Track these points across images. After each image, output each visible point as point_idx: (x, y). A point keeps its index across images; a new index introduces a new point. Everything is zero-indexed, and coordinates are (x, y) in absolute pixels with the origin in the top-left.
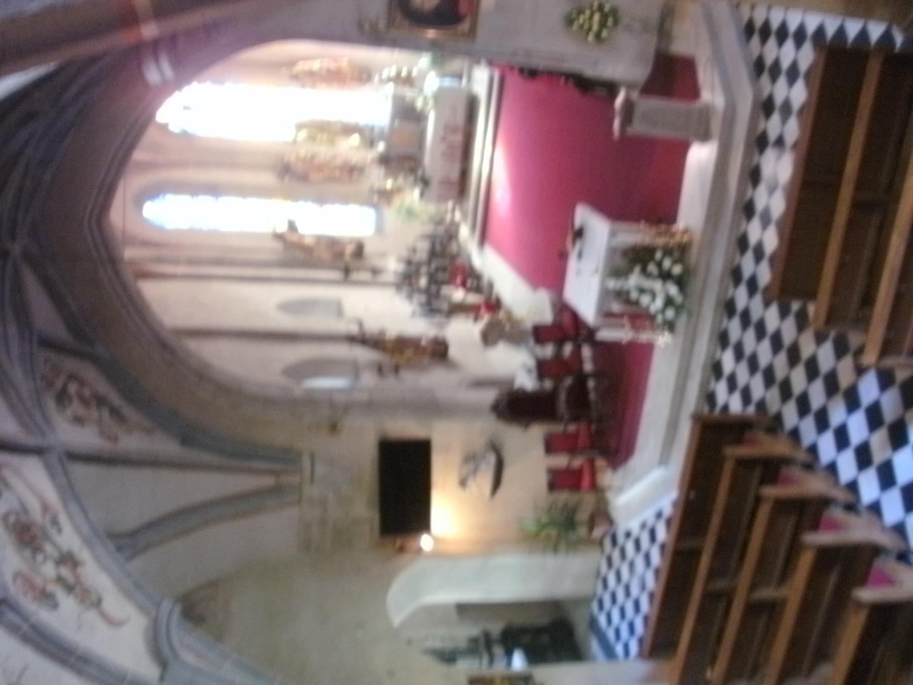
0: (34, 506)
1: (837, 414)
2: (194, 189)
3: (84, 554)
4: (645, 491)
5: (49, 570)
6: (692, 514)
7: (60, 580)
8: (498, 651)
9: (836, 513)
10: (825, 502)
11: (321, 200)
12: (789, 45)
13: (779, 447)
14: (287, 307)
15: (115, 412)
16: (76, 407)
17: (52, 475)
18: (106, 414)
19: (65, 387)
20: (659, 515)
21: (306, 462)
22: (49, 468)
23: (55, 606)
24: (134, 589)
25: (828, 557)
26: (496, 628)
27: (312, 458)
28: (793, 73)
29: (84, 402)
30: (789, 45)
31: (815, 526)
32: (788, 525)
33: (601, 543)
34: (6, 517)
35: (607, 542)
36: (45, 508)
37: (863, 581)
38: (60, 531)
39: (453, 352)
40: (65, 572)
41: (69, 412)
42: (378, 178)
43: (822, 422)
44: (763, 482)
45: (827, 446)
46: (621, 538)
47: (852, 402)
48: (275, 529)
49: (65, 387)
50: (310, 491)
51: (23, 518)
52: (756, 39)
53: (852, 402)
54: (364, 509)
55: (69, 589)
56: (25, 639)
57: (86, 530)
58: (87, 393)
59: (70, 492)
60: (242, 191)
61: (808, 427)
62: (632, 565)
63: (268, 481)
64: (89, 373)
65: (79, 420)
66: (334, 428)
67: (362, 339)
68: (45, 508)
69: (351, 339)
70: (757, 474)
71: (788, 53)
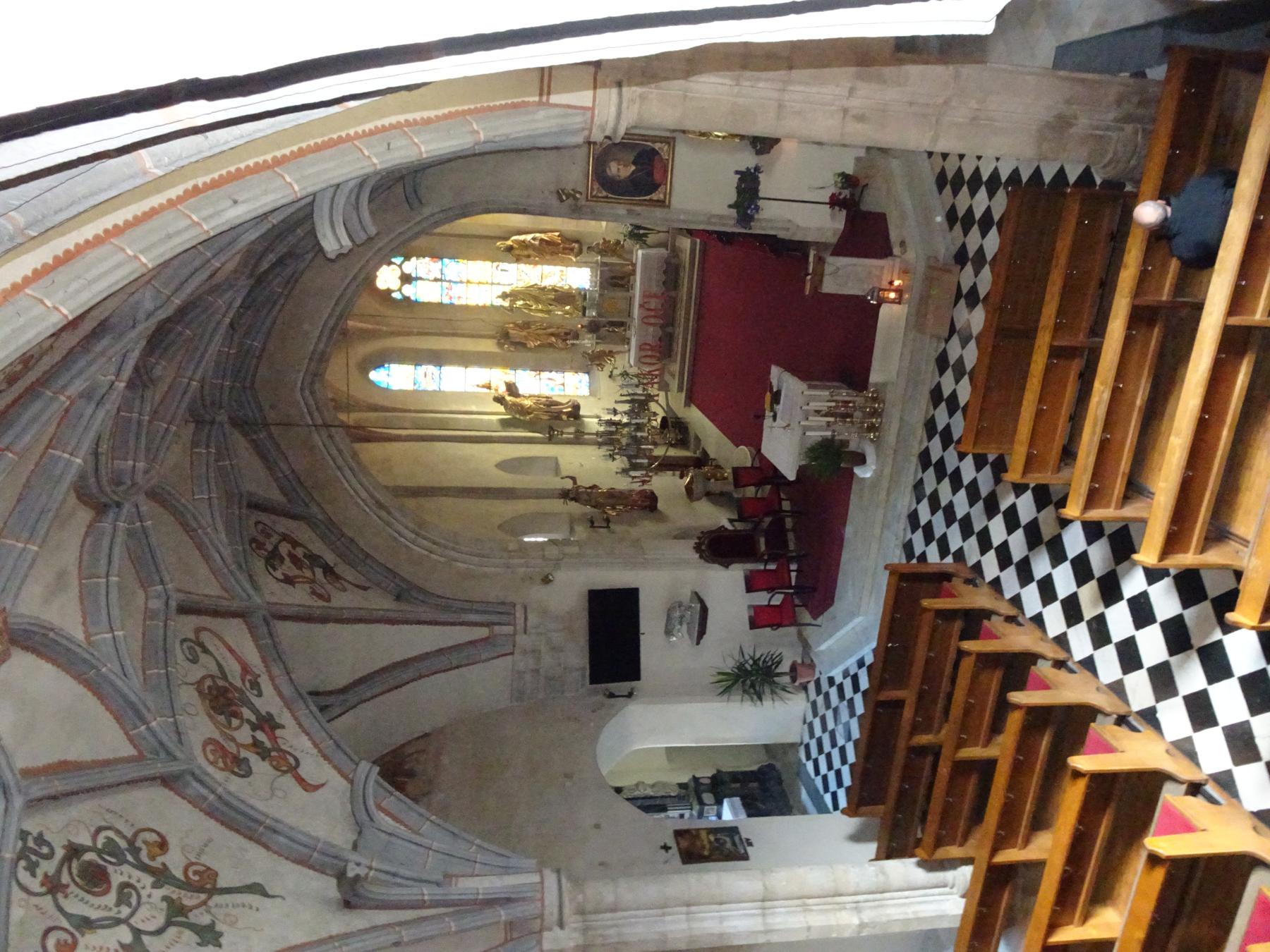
0: (233, 668)
1: (1041, 566)
2: (418, 358)
3: (285, 718)
4: (850, 635)
5: (244, 735)
6: (891, 661)
7: (256, 744)
8: (708, 798)
9: (1043, 669)
10: (1031, 658)
11: (538, 368)
12: (982, 193)
13: (980, 599)
14: (504, 465)
15: (328, 570)
16: (288, 568)
17: (255, 638)
18: (319, 571)
19: (276, 547)
20: (861, 664)
21: (519, 614)
22: (252, 630)
23: (248, 773)
24: (338, 753)
25: (1039, 717)
26: (706, 773)
27: (525, 608)
28: (986, 223)
29: (295, 560)
30: (982, 193)
31: (1021, 686)
32: (994, 680)
33: (804, 688)
34: (200, 683)
35: (812, 687)
36: (246, 669)
37: (1076, 748)
38: (260, 695)
39: (660, 505)
40: (261, 736)
41: (279, 574)
42: (588, 342)
43: (1025, 574)
44: (965, 636)
45: (1031, 598)
46: (825, 685)
47: (1058, 556)
48: (486, 683)
49: (276, 547)
50: (521, 640)
51: (221, 683)
52: (948, 190)
53: (1058, 556)
54: (577, 656)
55: (264, 754)
56: (211, 813)
57: (287, 690)
58: (299, 552)
59: (273, 653)
60: (465, 359)
61: (1010, 580)
62: (836, 711)
63: (483, 632)
64: (303, 533)
65: (289, 580)
66: (546, 580)
67: (571, 495)
68: (246, 669)
69: (565, 495)
70: (958, 625)
71: (981, 201)
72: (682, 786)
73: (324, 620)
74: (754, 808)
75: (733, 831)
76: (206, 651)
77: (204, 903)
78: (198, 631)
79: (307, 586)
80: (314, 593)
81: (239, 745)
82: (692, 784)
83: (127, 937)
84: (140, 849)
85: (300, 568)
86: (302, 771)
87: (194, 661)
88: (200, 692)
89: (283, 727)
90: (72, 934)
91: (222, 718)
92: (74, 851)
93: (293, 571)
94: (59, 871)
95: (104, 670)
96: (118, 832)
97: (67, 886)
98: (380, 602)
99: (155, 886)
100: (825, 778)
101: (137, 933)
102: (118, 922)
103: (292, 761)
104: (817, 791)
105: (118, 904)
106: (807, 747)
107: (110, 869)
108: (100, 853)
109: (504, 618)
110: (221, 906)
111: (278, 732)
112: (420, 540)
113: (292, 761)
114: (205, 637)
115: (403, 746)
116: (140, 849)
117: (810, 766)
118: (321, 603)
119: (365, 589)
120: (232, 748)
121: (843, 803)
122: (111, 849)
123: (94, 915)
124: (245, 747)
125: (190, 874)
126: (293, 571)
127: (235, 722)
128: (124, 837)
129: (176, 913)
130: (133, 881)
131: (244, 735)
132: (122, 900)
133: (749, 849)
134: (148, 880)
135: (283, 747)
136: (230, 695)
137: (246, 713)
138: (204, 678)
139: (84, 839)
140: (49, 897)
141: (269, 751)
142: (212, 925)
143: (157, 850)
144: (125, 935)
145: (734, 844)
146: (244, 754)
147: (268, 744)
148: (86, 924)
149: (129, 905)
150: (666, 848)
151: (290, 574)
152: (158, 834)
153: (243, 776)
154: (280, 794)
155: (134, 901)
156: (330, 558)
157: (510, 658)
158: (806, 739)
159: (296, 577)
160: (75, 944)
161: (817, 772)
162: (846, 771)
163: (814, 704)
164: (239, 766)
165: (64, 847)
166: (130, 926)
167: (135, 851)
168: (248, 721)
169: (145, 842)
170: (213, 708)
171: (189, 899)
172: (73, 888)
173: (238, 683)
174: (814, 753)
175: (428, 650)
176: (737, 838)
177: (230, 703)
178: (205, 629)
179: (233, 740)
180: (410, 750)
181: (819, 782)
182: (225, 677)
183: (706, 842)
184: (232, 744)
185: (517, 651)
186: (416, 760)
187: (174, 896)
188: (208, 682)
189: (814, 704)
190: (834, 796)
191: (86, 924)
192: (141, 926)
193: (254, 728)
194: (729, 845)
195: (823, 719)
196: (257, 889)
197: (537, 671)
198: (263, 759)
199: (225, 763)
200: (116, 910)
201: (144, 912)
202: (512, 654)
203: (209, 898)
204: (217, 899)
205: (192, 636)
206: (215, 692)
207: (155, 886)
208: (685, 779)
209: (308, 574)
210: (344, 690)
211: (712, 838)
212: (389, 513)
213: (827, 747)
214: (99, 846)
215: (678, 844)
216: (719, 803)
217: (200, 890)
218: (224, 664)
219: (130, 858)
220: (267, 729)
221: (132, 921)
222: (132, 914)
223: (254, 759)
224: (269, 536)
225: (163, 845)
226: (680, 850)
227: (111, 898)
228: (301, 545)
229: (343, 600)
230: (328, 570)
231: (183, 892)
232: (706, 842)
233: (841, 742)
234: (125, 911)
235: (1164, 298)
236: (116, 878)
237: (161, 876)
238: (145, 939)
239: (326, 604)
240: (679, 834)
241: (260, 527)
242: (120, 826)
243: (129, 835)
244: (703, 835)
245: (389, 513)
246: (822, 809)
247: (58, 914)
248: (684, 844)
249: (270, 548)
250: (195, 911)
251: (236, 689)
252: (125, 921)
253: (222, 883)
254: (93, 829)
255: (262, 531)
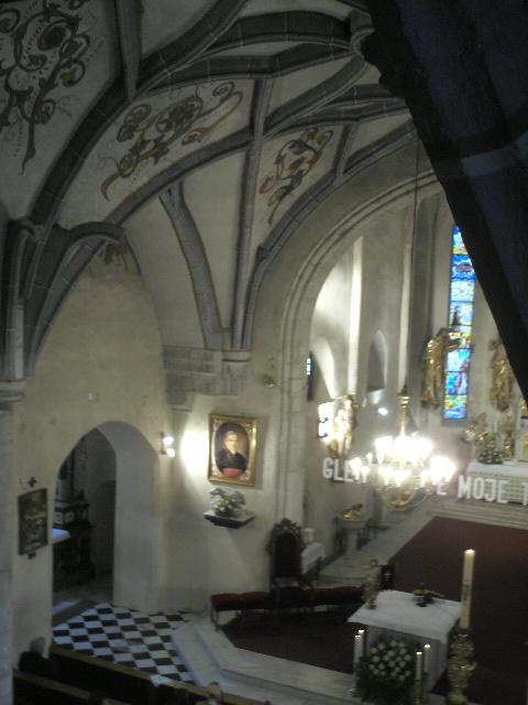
0: (208, 122)
7: (144, 143)
8: (70, 517)
16: (291, 158)
19: (310, 148)
21: (243, 355)
26: (90, 515)
34: (197, 98)
36: (205, 131)
38: (184, 143)
40: (150, 146)
41: (286, 151)
46: (164, 632)
49: (310, 148)
51: (196, 113)
55: (135, 150)
58: (305, 166)
62: (139, 641)
64: (322, 169)
65: (280, 159)
68: (205, 131)
72: (81, 496)
73: (244, 186)
74: (61, 551)
75: (44, 540)
76: (223, 101)
77: (24, 117)
78: (240, 94)
79: (274, 174)
80: (268, 180)
81: (143, 131)
82: (82, 503)
83: (6, 65)
84: (69, 67)
85: (291, 167)
86: (120, 179)
87: (215, 93)
88: (189, 99)
89: (156, 162)
90: (11, 29)
91: (167, 116)
92: (73, 23)
93: (288, 162)
94: (61, 14)
95: (212, 35)
96: (84, 51)
97: (48, 21)
98: (257, 235)
99: (41, 80)
100: (80, 625)
101: (8, 72)
102: (18, 58)
103: (127, 172)
104: (71, 617)
105: (31, 57)
106: (108, 611)
107: (58, 49)
108: (71, 40)
109: (238, 343)
110: (21, 129)
111: (152, 159)
112: (311, 268)
113: (127, 172)
114: (235, 99)
115: (132, 251)
116: (69, 67)
117: (92, 612)
118: (259, 185)
119: (270, 221)
120: (142, 125)
121: (61, 640)
122: (74, 46)
123: (25, 43)
124: (142, 135)
125: (49, 104)
126: (288, 162)
127: (162, 127)
128: (80, 55)
129: (20, 97)
130: (47, 65)
131: (152, 134)
132: (33, 60)
133: (26, 556)
134: (46, 75)
135: (139, 164)
136: (185, 121)
137: (171, 133)
138: (201, 101)
139: (82, 28)
140: (41, 9)
141: (137, 154)
142: (8, 124)
143: (67, 79)
144: (9, 62)
145: (34, 541)
146: (137, 135)
147: (143, 152)
148: (18, 38)
149: (29, 65)
150: (32, 482)
151: (285, 160)
152: (79, 79)
153: (119, 135)
154: (102, 164)
155: (33, 67)
156: (298, 192)
157: (202, 346)
158: (117, 611)
159: (283, 164)
160: (6, 31)
161: (88, 619)
162: (86, 646)
163: (145, 621)
164: (126, 132)
165: (77, 16)
166: (14, 67)
167: (67, 65)
168: (163, 136)
169: (75, 70)
170: (175, 110)
171: (28, 106)
172: (47, 24)
173: (195, 126)
174: (104, 617)
175: (216, 288)
176: (38, 544)
177: (179, 122)
178: (241, 100)
179: (149, 126)
180: (128, 257)
181: (78, 619)
182: (200, 116)
183: (36, 516)
184: (145, 125)
185: (208, 352)
186: (120, 265)
187: (32, 95)
188: (196, 104)
189: (145, 621)
190: (65, 633)
191: (18, 38)
192: (13, 74)
193: (157, 141)
194: (33, 537)
195: (132, 628)
196: (31, 152)
197: (189, 367)
198: (131, 150)
199: (130, 121)
200: (27, 55)
201: (23, 74)
202: (206, 348)
203: (27, 119)
204: (26, 124)
205: (236, 89)
206: (189, 109)
207: (41, 80)
208: (87, 496)
209: (285, 174)
210: (183, 205)
211: (39, 522)
212: (337, 241)
213: (109, 630)
214: (75, 39)
215: (36, 492)
216: (65, 527)
217: (35, 112)
218: (213, 113)
219: (64, 61)
220: (156, 150)
221: (17, 68)
222: (21, 67)
223: (131, 143)
224: (319, 143)
225: (71, 83)
226: (31, 493)
227: (36, 51)
228: (310, 168)
229: (261, 205)
230: (288, 189)
231: (34, 101)
232: (36, 516)
233: (113, 643)
234: (24, 62)
235: (472, 649)
236: (48, 54)
237: (48, 84)
238: (4, 78)
239: (258, 188)
240: (44, 492)
241: (328, 135)
242: (90, 52)
243: (82, 59)
244: (42, 515)
245: (337, 241)
246: (57, 619)
247: (29, 17)
248: (35, 498)
249: (310, 143)
250: (19, 112)
251: (189, 127)
252: (18, 63)
253: (37, 126)
254: (88, 34)
255: (324, 137)
